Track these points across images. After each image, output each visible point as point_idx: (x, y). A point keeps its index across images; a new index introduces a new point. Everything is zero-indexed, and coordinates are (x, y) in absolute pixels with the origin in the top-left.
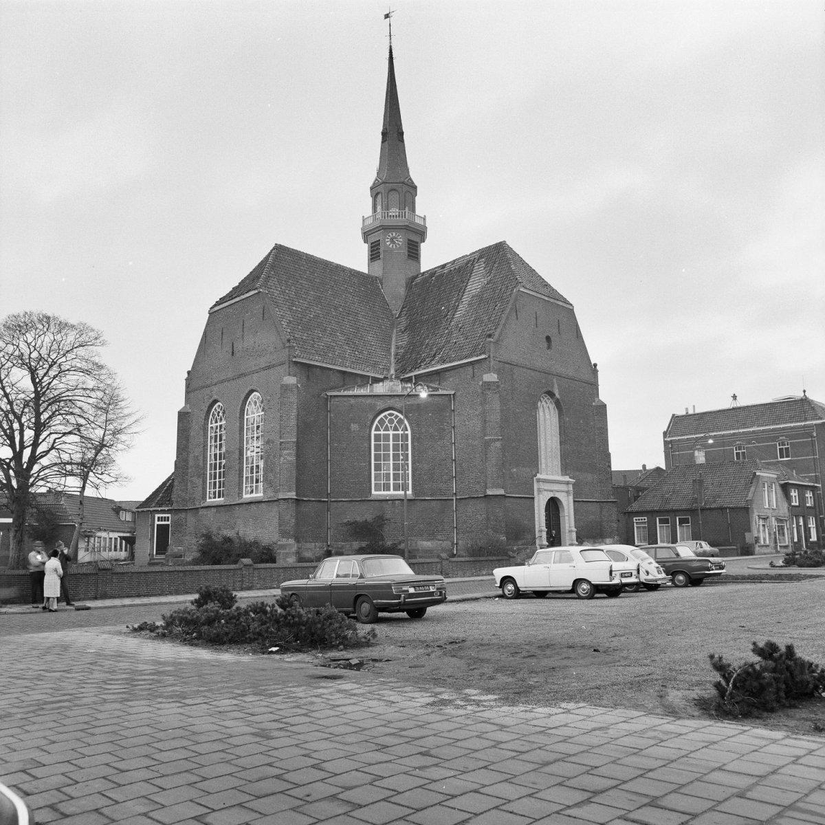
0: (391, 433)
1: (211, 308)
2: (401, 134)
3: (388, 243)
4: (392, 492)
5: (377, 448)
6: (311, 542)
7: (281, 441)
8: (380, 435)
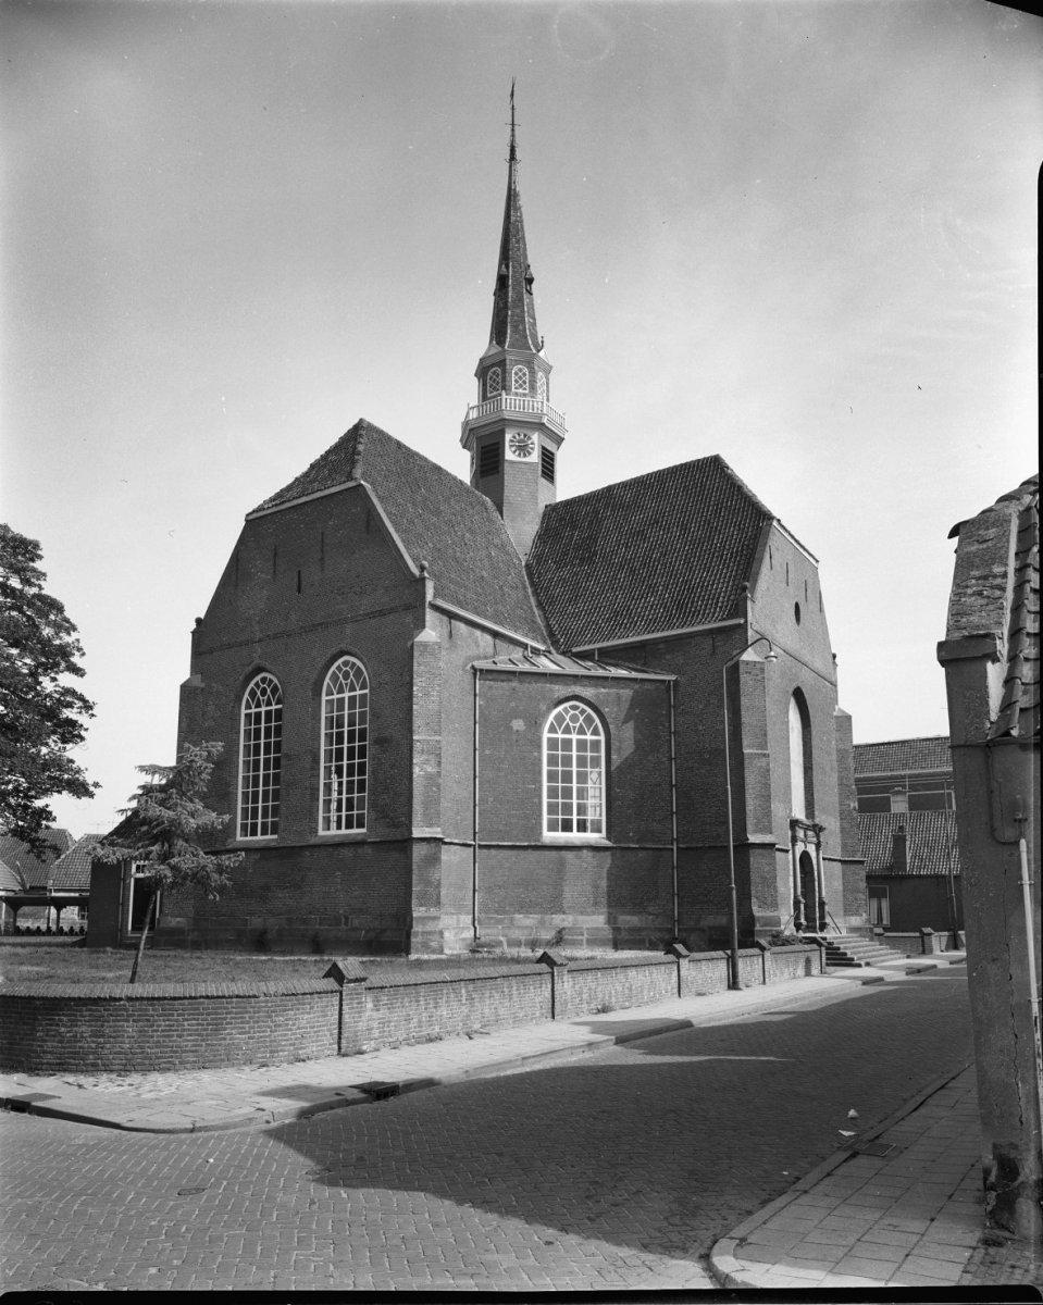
0: (574, 737)
1: (247, 515)
4: (259, 837)
5: (552, 760)
6: (453, 914)
7: (438, 738)
8: (586, 741)
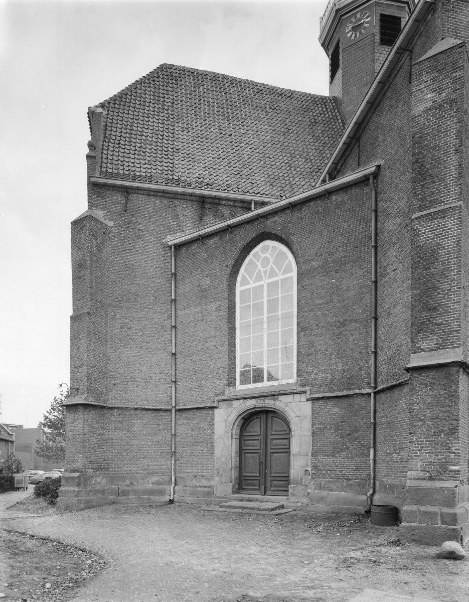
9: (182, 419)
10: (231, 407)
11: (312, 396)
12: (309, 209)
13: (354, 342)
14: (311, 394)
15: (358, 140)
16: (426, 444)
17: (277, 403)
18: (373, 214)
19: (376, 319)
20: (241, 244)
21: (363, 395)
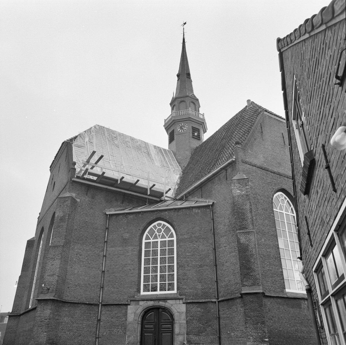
2: (189, 75)
3: (179, 130)
4: (158, 292)
9: (105, 310)
10: (139, 304)
11: (186, 301)
12: (182, 212)
13: (206, 276)
14: (185, 300)
15: (201, 188)
16: (253, 328)
17: (167, 304)
18: (212, 220)
19: (216, 266)
20: (148, 221)
21: (212, 302)
